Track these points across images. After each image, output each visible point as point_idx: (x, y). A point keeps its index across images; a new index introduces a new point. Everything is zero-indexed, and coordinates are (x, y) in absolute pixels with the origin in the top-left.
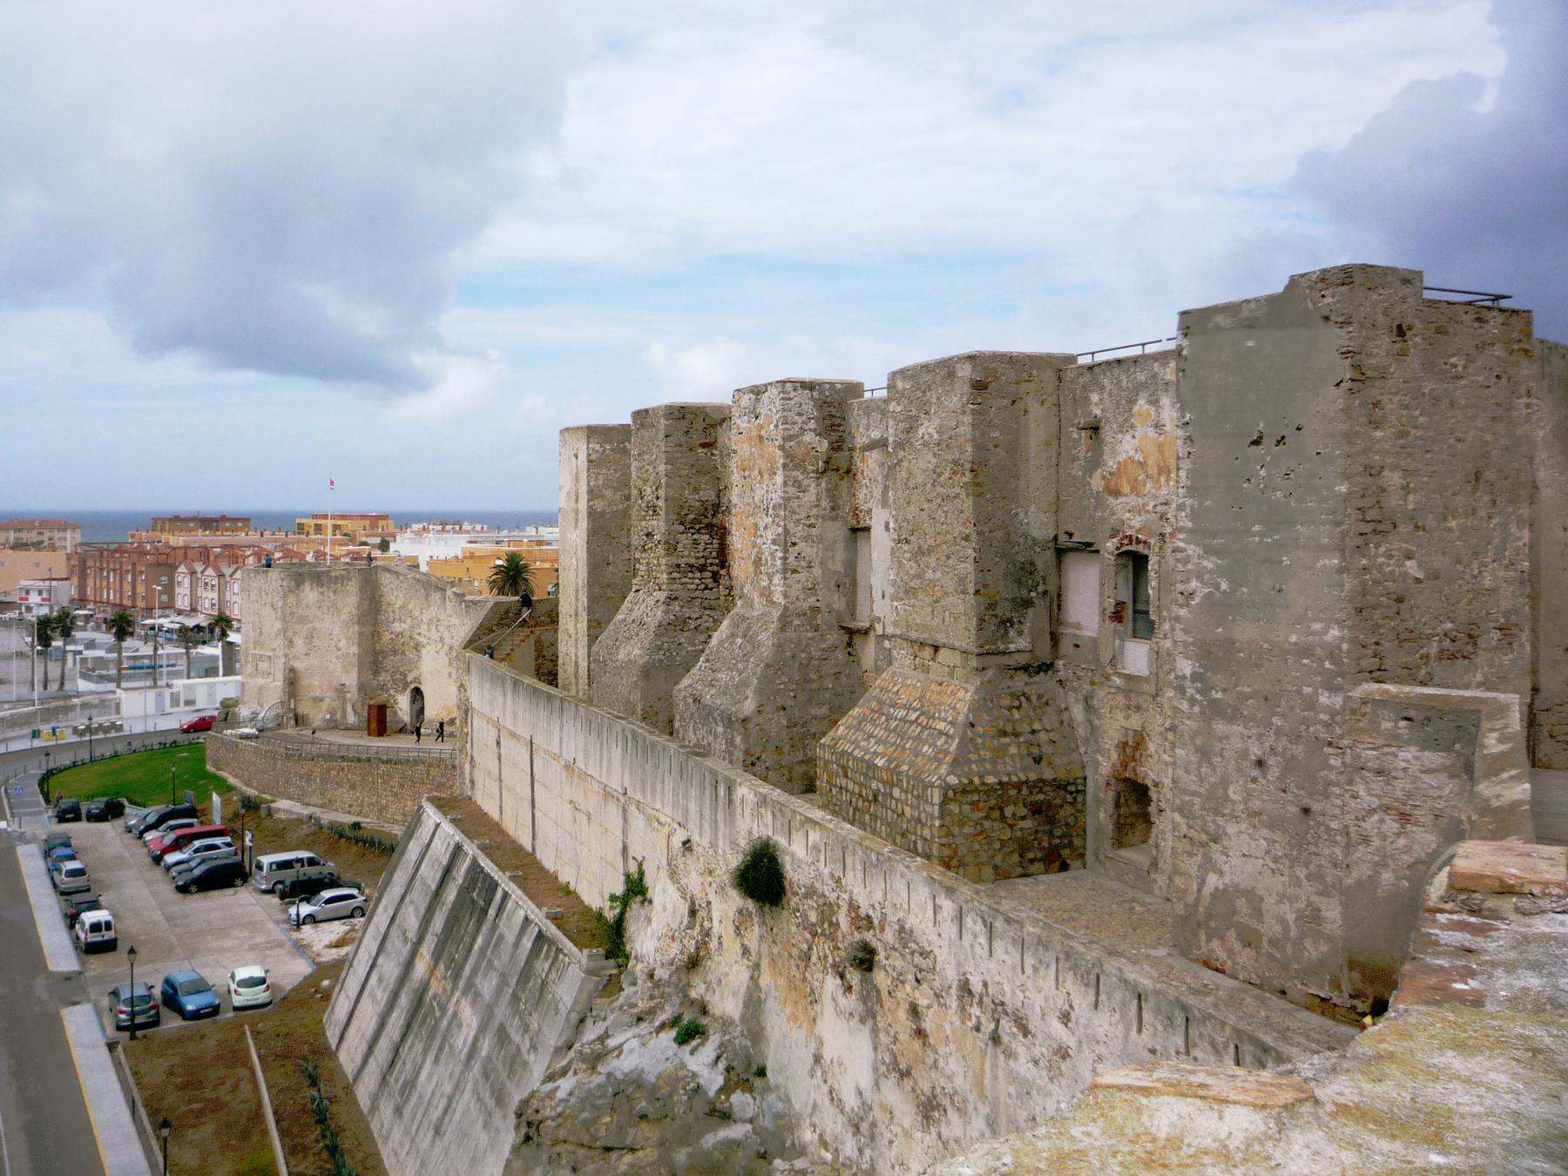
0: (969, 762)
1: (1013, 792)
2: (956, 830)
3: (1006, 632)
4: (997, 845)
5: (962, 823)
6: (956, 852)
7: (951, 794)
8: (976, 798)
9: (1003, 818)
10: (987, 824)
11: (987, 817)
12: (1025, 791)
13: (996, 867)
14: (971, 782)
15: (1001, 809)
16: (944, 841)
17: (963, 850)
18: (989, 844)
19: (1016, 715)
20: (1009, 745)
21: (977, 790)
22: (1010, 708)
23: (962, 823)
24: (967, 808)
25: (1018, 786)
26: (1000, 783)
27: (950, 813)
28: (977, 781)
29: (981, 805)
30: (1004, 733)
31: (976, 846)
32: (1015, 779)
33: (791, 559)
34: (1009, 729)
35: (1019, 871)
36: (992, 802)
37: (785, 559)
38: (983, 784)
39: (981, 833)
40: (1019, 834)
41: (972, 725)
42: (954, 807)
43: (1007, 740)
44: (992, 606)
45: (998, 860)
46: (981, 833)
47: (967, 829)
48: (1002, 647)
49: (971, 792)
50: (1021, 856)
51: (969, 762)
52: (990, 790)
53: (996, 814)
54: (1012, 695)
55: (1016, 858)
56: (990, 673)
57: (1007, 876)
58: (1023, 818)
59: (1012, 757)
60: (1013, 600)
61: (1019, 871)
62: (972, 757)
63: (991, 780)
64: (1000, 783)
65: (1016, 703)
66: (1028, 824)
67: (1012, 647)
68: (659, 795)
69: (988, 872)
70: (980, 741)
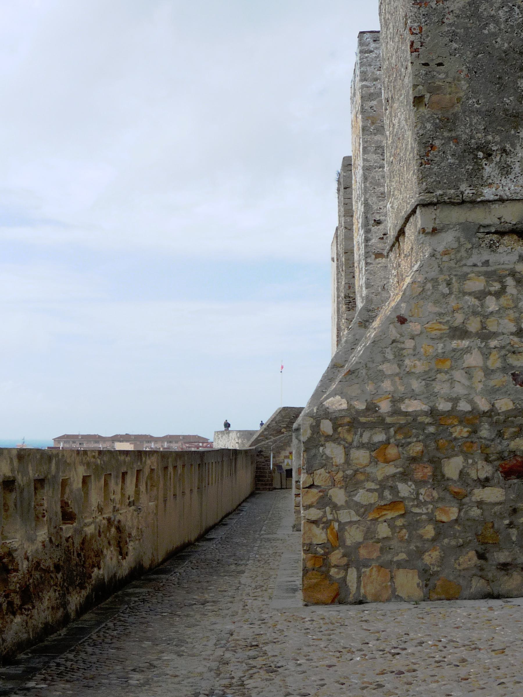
0: (381, 376)
1: (460, 432)
2: (339, 496)
3: (479, 168)
4: (429, 531)
5: (351, 483)
6: (339, 537)
7: (327, 427)
8: (380, 437)
9: (439, 479)
10: (405, 489)
11: (405, 476)
12: (485, 431)
13: (427, 575)
14: (371, 408)
15: (436, 463)
16: (314, 514)
17: (354, 536)
18: (413, 525)
19: (492, 304)
20: (468, 350)
21: (381, 423)
22: (481, 295)
23: (351, 483)
24: (361, 456)
25: (473, 419)
26: (433, 412)
27: (327, 463)
28: (385, 407)
29: (392, 451)
30: (460, 332)
31: (383, 530)
32: (464, 406)
33: (374, 241)
34: (474, 326)
35: (478, 584)
36: (416, 448)
37: (367, 240)
38: (396, 412)
39: (393, 504)
40: (475, 512)
41: (402, 320)
42: (334, 452)
43: (466, 343)
44: (447, 122)
45: (431, 557)
46: (393, 504)
47: (362, 497)
48: (468, 192)
49: (370, 426)
50: (481, 556)
51: (381, 376)
52: (410, 425)
53: (424, 471)
54: (489, 276)
55: (469, 559)
56: (448, 239)
57: (452, 595)
58: (485, 483)
59: (468, 372)
60: (489, 114)
61: (478, 584)
62: (388, 368)
63: (413, 406)
64: (433, 412)
65: (496, 286)
66: (493, 494)
67: (488, 193)
68: (204, 467)
69: (408, 581)
70: (409, 344)
